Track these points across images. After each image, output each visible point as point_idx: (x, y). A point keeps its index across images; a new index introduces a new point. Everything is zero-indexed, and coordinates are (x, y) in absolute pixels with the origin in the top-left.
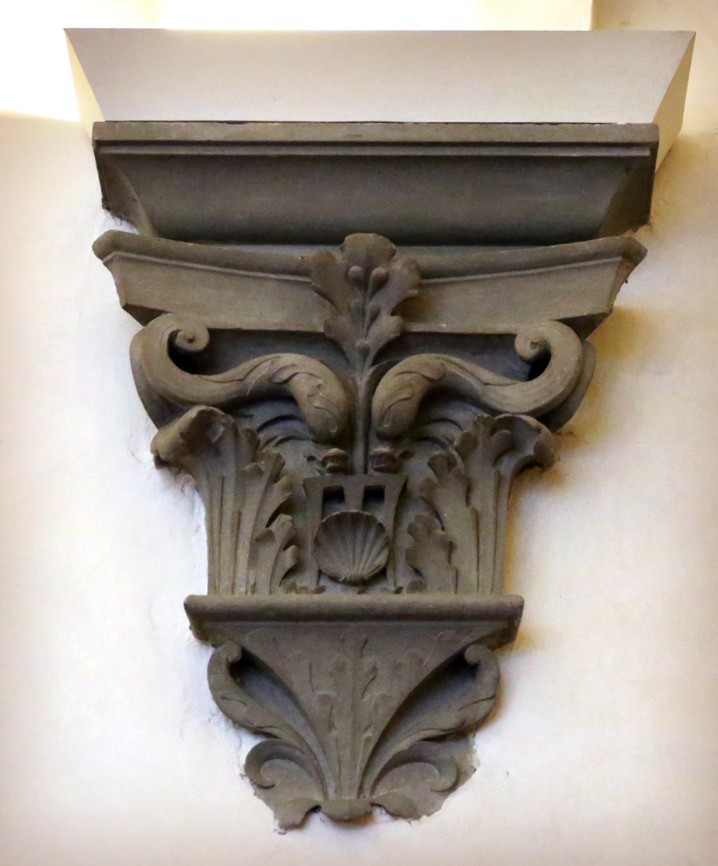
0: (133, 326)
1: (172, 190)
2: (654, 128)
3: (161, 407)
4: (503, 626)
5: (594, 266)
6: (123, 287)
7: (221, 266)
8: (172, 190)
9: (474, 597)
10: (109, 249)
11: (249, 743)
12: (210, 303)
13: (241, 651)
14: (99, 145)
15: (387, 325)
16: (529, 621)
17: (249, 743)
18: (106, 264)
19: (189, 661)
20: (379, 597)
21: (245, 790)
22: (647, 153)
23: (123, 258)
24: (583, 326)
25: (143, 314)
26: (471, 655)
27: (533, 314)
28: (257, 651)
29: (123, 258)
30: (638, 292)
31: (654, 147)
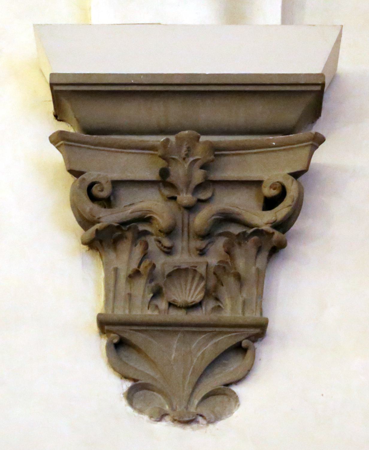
0: (71, 179)
1: (89, 109)
2: (322, 75)
3: (85, 222)
4: (259, 330)
5: (255, 153)
6: (68, 160)
7: (117, 148)
8: (89, 109)
9: (251, 316)
10: (60, 140)
11: (128, 384)
12: (110, 166)
13: (120, 337)
14: (52, 85)
15: (198, 176)
16: (273, 327)
17: (128, 384)
18: (58, 148)
19: (97, 346)
20: (197, 316)
21: (124, 402)
22: (318, 88)
23: (65, 144)
24: (296, 175)
25: (76, 173)
26: (244, 344)
27: (271, 168)
28: (126, 336)
29: (65, 144)
30: (321, 157)
31: (323, 85)
